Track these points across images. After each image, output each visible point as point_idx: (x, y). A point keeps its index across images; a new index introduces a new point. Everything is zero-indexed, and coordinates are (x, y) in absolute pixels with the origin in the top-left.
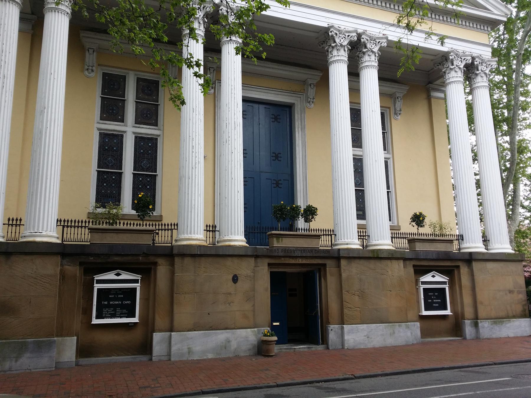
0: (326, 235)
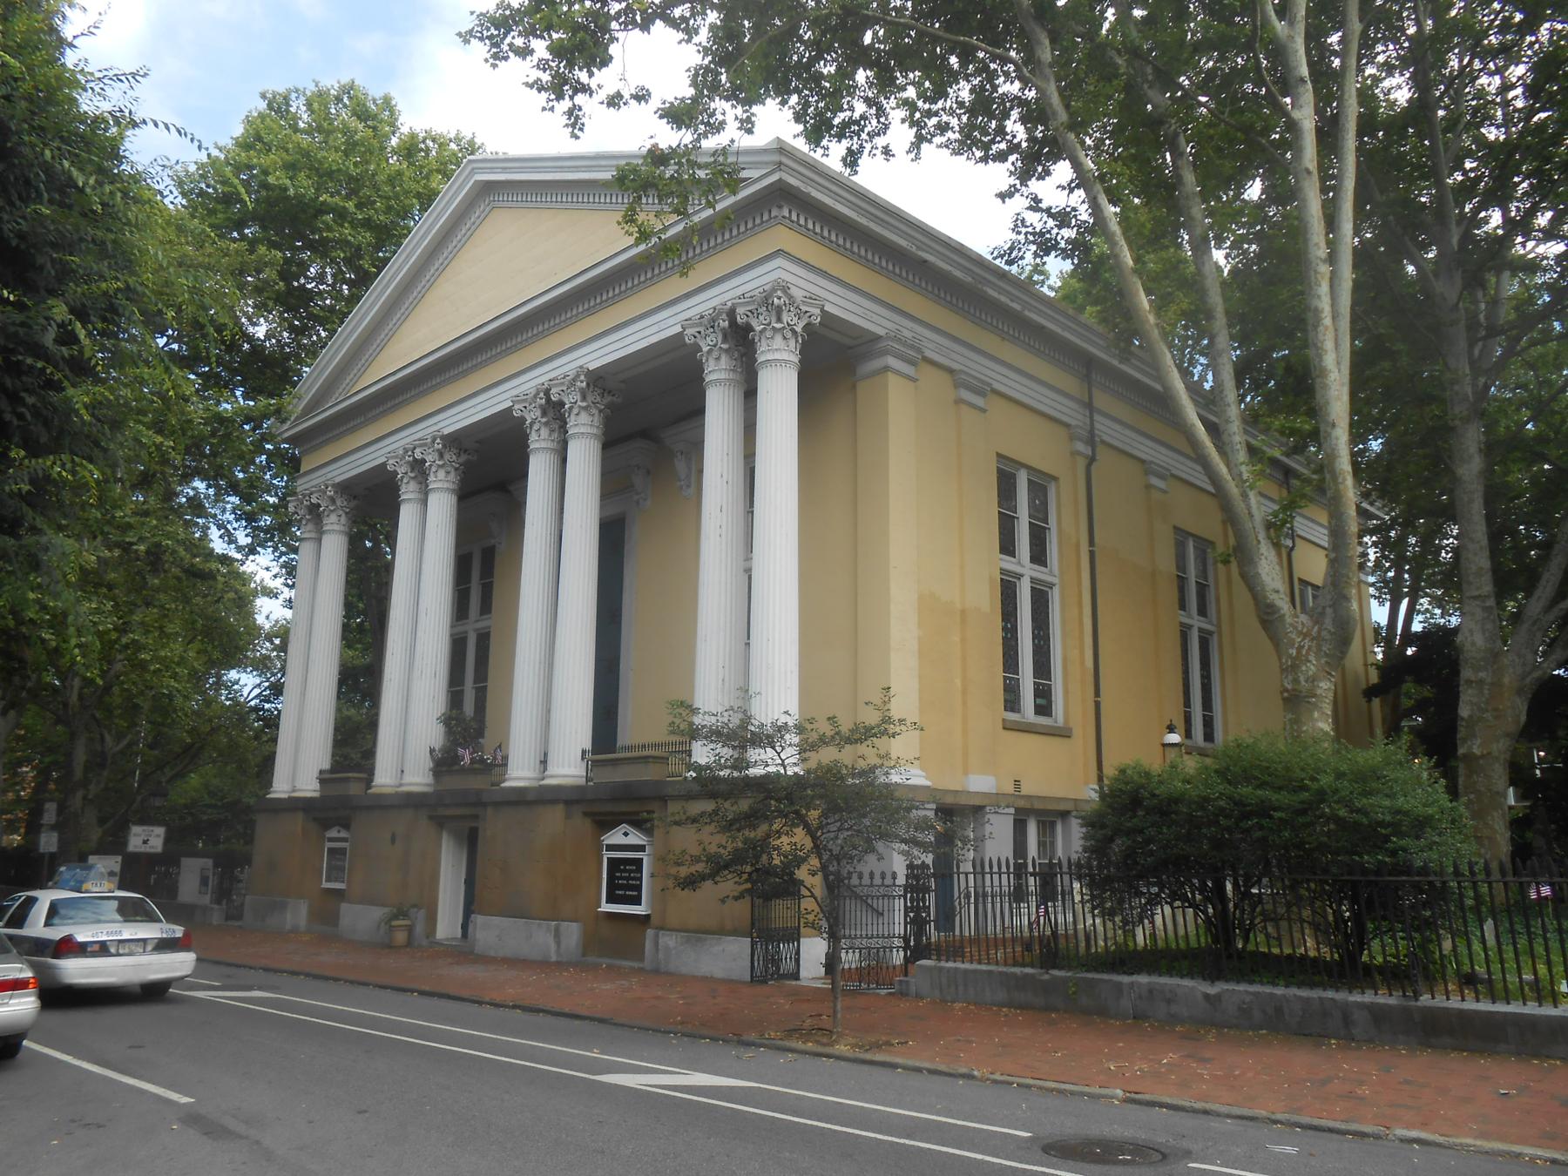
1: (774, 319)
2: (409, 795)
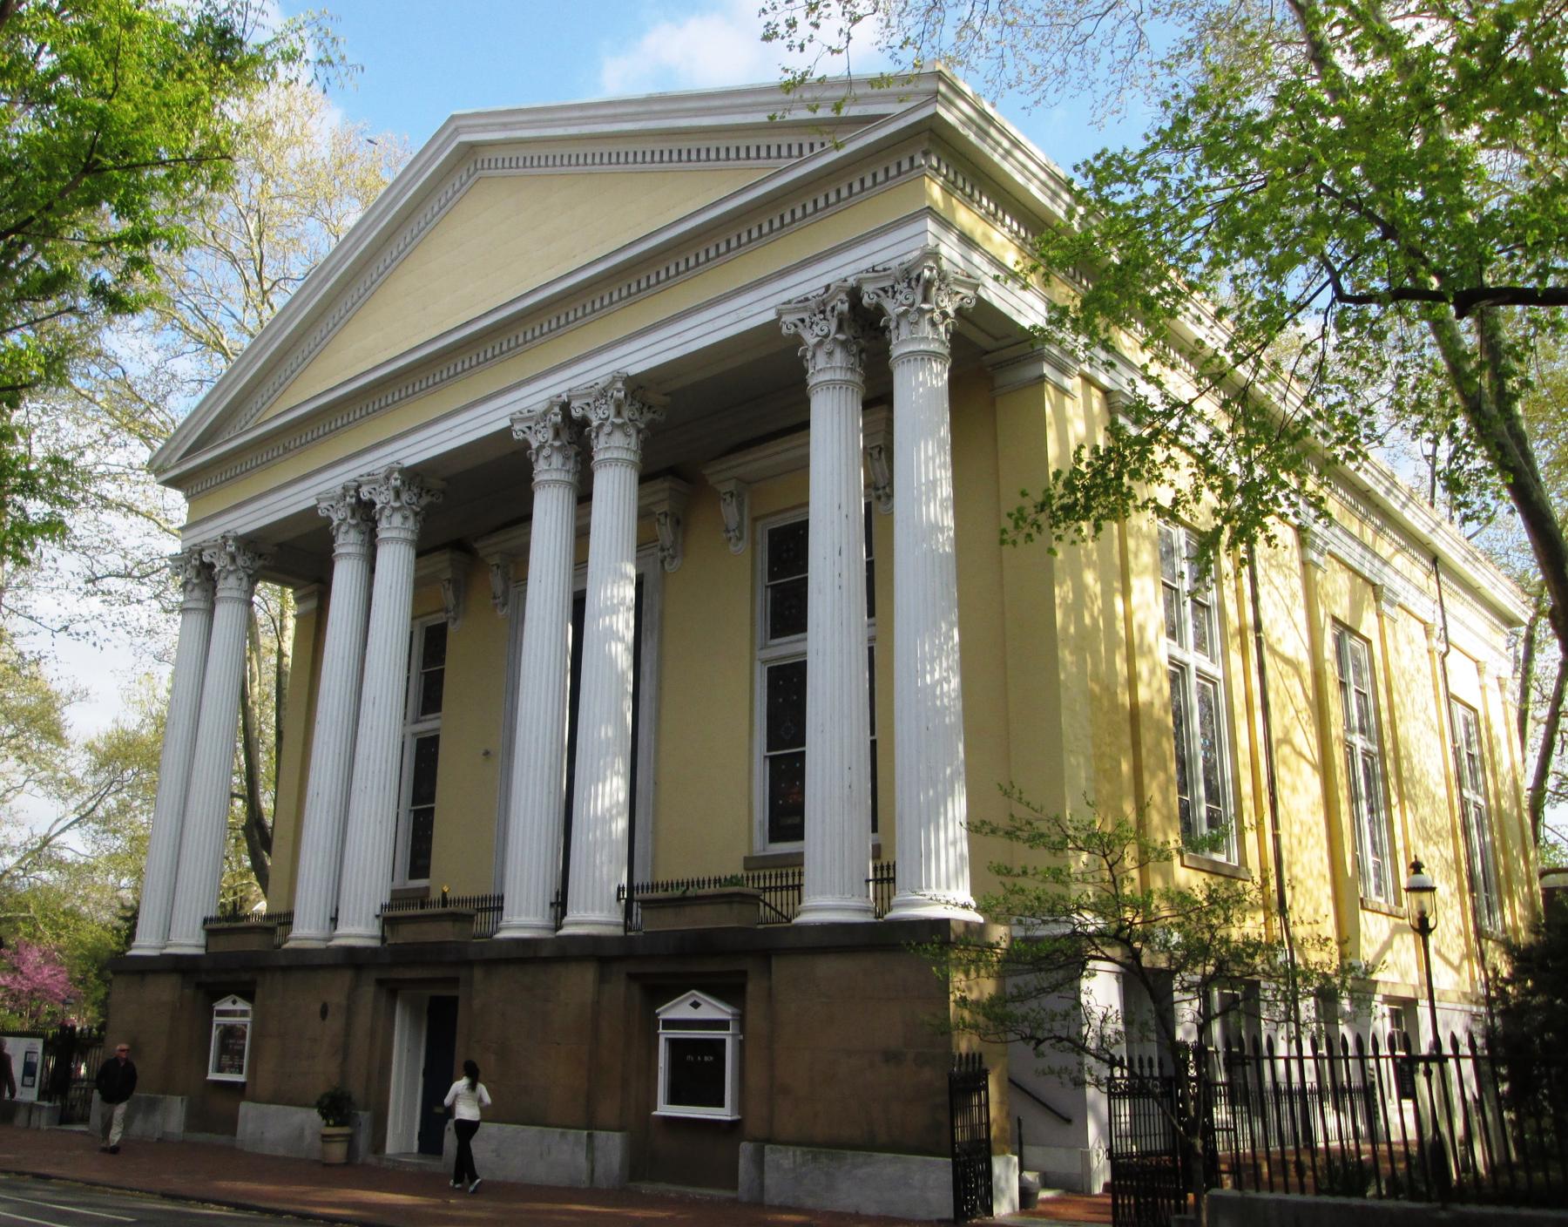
0: (787, 887)
1: (919, 298)
2: (350, 951)
